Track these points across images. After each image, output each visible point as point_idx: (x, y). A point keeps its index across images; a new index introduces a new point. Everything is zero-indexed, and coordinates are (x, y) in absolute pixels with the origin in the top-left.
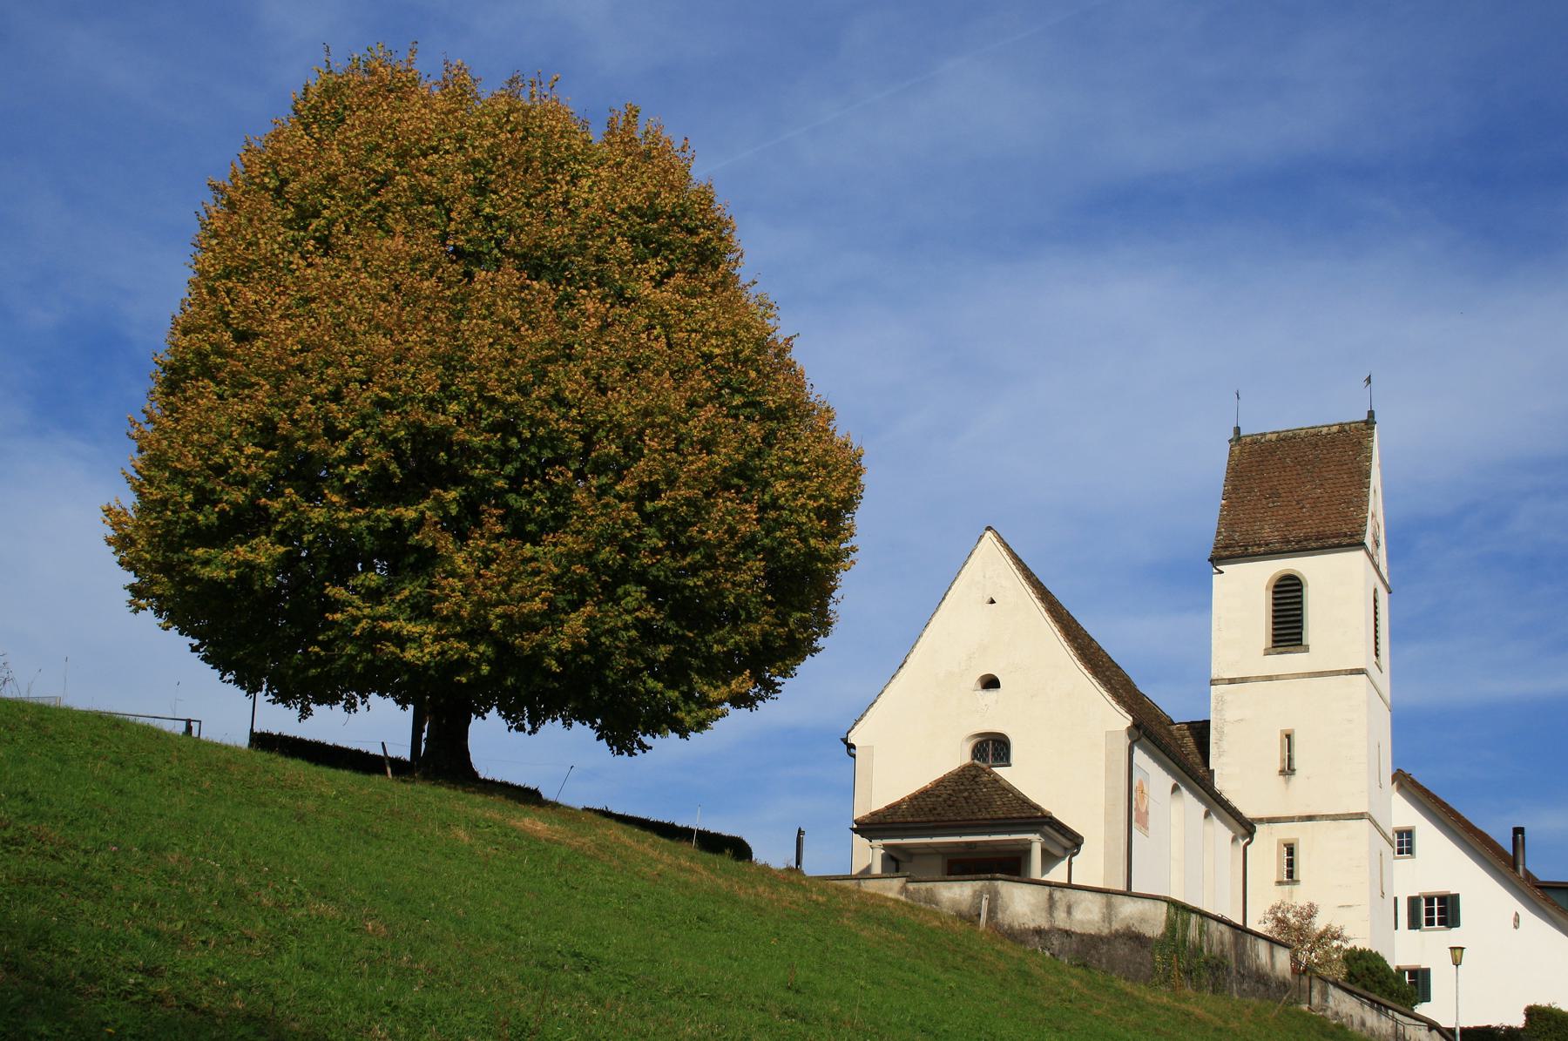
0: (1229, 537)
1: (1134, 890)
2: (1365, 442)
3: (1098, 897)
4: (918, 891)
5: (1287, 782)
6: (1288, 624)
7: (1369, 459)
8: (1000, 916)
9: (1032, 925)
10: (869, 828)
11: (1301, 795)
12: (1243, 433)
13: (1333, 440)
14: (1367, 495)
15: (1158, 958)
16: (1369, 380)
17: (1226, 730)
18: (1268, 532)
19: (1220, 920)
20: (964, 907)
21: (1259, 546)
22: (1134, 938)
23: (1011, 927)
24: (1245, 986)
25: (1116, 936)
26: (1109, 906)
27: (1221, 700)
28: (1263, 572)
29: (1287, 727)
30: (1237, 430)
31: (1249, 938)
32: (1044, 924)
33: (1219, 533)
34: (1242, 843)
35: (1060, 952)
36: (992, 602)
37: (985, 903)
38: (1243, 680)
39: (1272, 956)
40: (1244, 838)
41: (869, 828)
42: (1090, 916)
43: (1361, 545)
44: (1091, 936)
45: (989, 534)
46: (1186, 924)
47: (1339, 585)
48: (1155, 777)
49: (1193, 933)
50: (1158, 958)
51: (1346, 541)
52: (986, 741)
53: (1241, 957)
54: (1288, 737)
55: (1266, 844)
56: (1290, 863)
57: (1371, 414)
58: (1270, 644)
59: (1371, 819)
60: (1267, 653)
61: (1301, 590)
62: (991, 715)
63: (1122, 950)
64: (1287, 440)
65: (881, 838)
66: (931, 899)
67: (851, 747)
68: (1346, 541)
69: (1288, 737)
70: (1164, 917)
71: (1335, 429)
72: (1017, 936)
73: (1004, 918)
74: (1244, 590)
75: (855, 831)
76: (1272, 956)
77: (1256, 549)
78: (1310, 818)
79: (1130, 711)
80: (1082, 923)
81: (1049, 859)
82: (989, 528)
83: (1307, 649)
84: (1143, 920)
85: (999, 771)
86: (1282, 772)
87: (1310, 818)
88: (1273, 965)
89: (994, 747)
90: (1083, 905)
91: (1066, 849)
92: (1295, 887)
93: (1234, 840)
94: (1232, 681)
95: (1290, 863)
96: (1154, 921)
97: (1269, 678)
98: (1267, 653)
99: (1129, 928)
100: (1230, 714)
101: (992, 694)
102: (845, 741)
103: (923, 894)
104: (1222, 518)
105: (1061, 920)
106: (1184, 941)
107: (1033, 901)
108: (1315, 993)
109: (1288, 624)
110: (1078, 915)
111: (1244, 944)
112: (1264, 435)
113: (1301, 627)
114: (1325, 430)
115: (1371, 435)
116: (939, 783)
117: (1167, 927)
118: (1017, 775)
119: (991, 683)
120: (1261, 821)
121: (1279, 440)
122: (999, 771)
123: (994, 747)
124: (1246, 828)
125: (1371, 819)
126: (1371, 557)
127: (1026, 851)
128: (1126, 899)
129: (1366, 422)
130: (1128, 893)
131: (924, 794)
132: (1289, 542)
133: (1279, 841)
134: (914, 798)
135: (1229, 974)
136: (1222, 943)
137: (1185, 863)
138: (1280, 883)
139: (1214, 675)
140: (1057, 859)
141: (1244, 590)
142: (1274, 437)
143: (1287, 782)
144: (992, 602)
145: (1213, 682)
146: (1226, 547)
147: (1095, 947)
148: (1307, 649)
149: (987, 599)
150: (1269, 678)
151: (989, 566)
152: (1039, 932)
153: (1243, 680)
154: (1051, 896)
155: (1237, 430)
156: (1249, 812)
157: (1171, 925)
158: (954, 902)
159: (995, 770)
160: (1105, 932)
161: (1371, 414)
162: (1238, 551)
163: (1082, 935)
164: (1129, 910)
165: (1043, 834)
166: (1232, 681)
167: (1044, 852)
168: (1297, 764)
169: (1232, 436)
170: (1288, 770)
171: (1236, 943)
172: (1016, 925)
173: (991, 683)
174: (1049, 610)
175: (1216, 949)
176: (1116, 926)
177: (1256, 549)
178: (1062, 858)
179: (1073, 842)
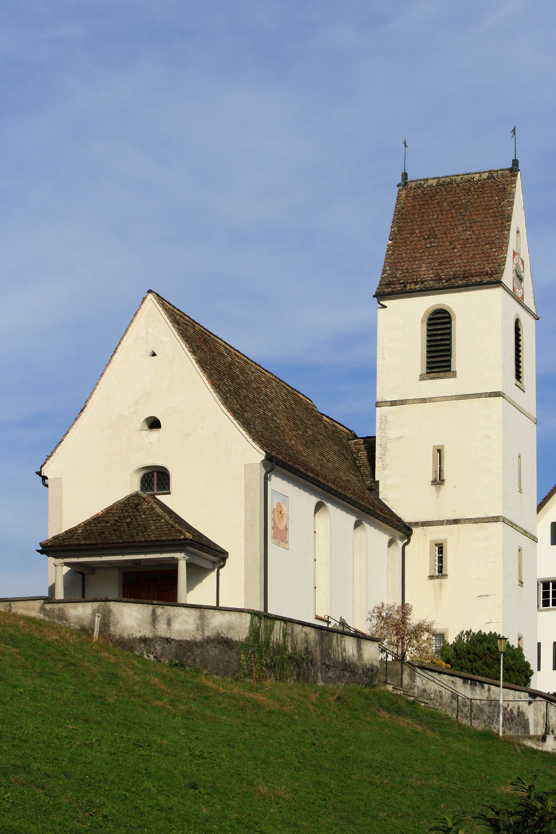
0: (393, 275)
1: (221, 605)
2: (508, 189)
3: (193, 612)
4: (52, 610)
5: (438, 490)
6: (439, 355)
7: (511, 204)
8: (112, 629)
9: (138, 635)
10: (53, 548)
11: (448, 504)
12: (409, 178)
13: (483, 186)
14: (507, 237)
15: (243, 657)
16: (514, 131)
17: (389, 446)
18: (425, 272)
19: (304, 624)
20: (86, 623)
21: (416, 283)
22: (223, 642)
23: (121, 637)
24: (330, 674)
25: (209, 641)
26: (202, 618)
27: (385, 420)
28: (418, 308)
29: (438, 443)
30: (405, 175)
31: (335, 636)
32: (149, 634)
33: (384, 271)
34: (400, 544)
35: (162, 655)
36: (154, 355)
37: (97, 620)
38: (403, 402)
39: (359, 649)
40: (402, 539)
41: (53, 548)
42: (186, 627)
43: (498, 283)
44: (187, 642)
45: (150, 296)
46: (270, 630)
47: (480, 318)
48: (294, 500)
49: (277, 635)
50: (243, 657)
51: (486, 279)
52: (152, 473)
53: (326, 652)
54: (439, 451)
55: (421, 543)
56: (441, 560)
57: (515, 162)
58: (425, 371)
59: (504, 520)
60: (422, 378)
61: (450, 323)
62: (155, 450)
63: (213, 652)
64: (446, 186)
65: (62, 557)
66: (62, 616)
67: (44, 478)
68: (486, 279)
69: (439, 451)
70: (248, 625)
71: (485, 176)
72: (126, 645)
73: (116, 630)
74: (403, 321)
75: (41, 552)
76: (359, 649)
77: (413, 286)
78: (456, 522)
79: (263, 446)
80: (179, 632)
81: (196, 573)
82: (150, 291)
83: (454, 375)
84: (230, 628)
85: (162, 498)
86: (434, 482)
87: (456, 522)
88: (360, 656)
89: (157, 478)
90: (180, 619)
91: (214, 562)
92: (444, 581)
93: (391, 543)
94: (393, 403)
95: (441, 560)
96: (240, 628)
97: (424, 401)
98: (422, 378)
99: (218, 634)
100: (392, 433)
101: (155, 434)
102: (39, 473)
103: (57, 612)
104: (388, 257)
105: (162, 630)
106: (267, 642)
107: (139, 616)
108: (406, 676)
109: (439, 355)
110: (177, 626)
111: (330, 642)
112: (426, 180)
113: (450, 355)
114: (477, 177)
115: (514, 182)
116: (109, 511)
117: (250, 633)
118: (178, 501)
119: (154, 424)
120: (417, 524)
121: (439, 185)
122: (162, 498)
123: (157, 478)
124: (403, 530)
125: (504, 520)
126: (513, 294)
127: (173, 566)
128: (216, 612)
129: (511, 170)
130: (217, 608)
131: (97, 519)
132: (440, 279)
133: (431, 541)
134: (88, 523)
135: (313, 665)
136: (307, 642)
137: (318, 572)
138: (431, 577)
139: (379, 398)
140: (206, 571)
141: (403, 321)
142: (434, 182)
143: (438, 490)
144: (154, 355)
145: (378, 404)
146: (389, 284)
147: (191, 650)
148: (454, 375)
149: (150, 352)
150: (424, 401)
151: (152, 326)
152: (144, 640)
153: (403, 402)
154: (154, 612)
155: (405, 175)
156: (407, 517)
157: (254, 632)
158: (79, 619)
159: (158, 497)
160: (199, 638)
161: (515, 162)
162: (398, 288)
163: (179, 641)
164: (218, 621)
165: (187, 552)
166: (393, 403)
167: (189, 565)
168: (446, 475)
169: (399, 180)
170: (520, 491)
171: (321, 641)
172: (125, 635)
173: (154, 424)
174: (203, 363)
175: (301, 647)
176: (208, 633)
177: (413, 286)
178: (212, 570)
179: (219, 556)
